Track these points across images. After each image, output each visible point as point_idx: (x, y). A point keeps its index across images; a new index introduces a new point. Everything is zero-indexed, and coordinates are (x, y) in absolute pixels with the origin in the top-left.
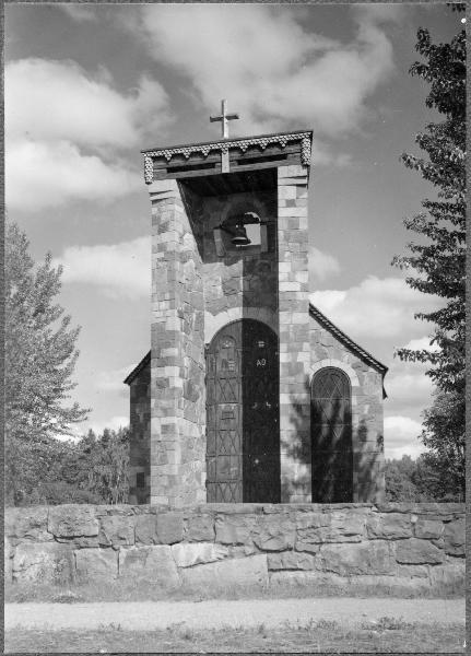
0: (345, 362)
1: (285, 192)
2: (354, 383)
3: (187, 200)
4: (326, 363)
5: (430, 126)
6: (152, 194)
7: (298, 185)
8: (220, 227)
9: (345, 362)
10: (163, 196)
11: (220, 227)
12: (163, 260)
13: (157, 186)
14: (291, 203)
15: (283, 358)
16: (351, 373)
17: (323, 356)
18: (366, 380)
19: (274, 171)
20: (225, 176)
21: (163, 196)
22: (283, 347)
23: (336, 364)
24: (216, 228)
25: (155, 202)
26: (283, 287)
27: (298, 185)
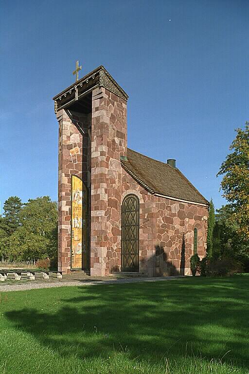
1: (95, 103)
2: (142, 202)
4: (130, 192)
6: (58, 118)
7: (100, 98)
13: (58, 114)
14: (97, 109)
16: (140, 196)
17: (127, 188)
19: (91, 93)
25: (59, 121)
27: (100, 98)
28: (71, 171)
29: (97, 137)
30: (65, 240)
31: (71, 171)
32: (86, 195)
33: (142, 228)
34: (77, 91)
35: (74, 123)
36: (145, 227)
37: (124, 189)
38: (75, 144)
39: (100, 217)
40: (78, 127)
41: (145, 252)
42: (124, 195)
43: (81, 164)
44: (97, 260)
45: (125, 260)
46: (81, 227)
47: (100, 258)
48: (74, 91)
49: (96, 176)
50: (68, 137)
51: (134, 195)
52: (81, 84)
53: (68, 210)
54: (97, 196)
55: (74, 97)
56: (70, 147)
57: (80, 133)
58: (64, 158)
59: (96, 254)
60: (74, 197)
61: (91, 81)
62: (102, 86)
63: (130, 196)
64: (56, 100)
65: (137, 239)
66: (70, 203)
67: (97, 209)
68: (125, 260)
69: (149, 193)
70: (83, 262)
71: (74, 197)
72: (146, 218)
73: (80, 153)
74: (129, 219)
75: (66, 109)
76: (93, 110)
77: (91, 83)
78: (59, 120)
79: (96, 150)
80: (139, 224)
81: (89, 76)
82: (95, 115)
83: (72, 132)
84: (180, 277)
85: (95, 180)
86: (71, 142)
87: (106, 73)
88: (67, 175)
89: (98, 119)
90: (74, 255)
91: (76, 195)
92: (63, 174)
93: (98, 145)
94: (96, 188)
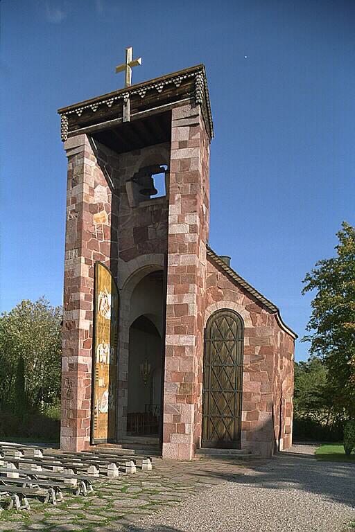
0: (239, 305)
1: (179, 133)
2: (248, 324)
3: (99, 155)
4: (222, 305)
5: (337, 247)
6: (68, 150)
7: (190, 126)
8: (132, 179)
9: (239, 305)
10: (76, 151)
11: (132, 179)
12: (73, 211)
13: (71, 142)
14: (183, 145)
15: (170, 299)
16: (245, 314)
17: (218, 298)
18: (259, 321)
19: (169, 113)
20: (124, 125)
21: (76, 151)
22: (170, 289)
23: (231, 306)
24: (128, 181)
25: (69, 157)
26: (174, 229)
27: (190, 126)
28: (95, 255)
29: (183, 196)
30: (82, 386)
31: (95, 255)
32: (116, 303)
33: (247, 370)
34: (129, 104)
35: (100, 164)
36: (254, 370)
37: (211, 299)
38: (101, 204)
39: (187, 349)
40: (105, 174)
41: (253, 415)
42: (211, 309)
43: (109, 244)
44: (181, 429)
45: (211, 426)
46: (108, 363)
47: (187, 426)
48: (121, 102)
49: (180, 269)
50: (92, 190)
51: (232, 311)
52: (142, 93)
53: (88, 329)
54: (182, 309)
55: (121, 113)
56: (94, 209)
57: (108, 187)
58: (85, 228)
59: (177, 418)
60: (100, 303)
61: (151, 97)
62: (200, 104)
63: (223, 313)
64: (66, 115)
65: (237, 390)
66: (94, 316)
67: (179, 331)
68: (211, 426)
69: (264, 311)
70: (160, 428)
71: (100, 303)
72: (257, 353)
73: (108, 224)
74: (222, 354)
75: (89, 136)
76: (174, 145)
77: (168, 94)
78: (70, 154)
79: (181, 220)
80: (242, 363)
81: (167, 80)
82: (177, 154)
83: (98, 182)
84: (340, 468)
85: (176, 277)
86: (95, 200)
87: (205, 80)
88: (88, 262)
89: (185, 163)
90: (97, 415)
91: (103, 302)
92: (83, 258)
93: (184, 212)
94: (179, 292)
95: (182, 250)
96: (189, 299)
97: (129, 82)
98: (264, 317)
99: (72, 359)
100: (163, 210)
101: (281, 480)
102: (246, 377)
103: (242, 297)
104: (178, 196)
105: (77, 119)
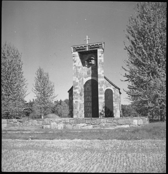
0: (111, 88)
2: (114, 92)
4: (108, 88)
6: (73, 55)
9: (111, 88)
13: (74, 53)
15: (99, 87)
16: (113, 90)
17: (107, 86)
22: (99, 85)
33: (114, 102)
42: (106, 89)
95: (101, 78)
96: (103, 87)
97: (87, 43)
98: (117, 90)
99: (76, 100)
100: (96, 71)
101: (132, 87)
102: (114, 103)
103: (112, 86)
104: (100, 67)
105: (76, 49)
